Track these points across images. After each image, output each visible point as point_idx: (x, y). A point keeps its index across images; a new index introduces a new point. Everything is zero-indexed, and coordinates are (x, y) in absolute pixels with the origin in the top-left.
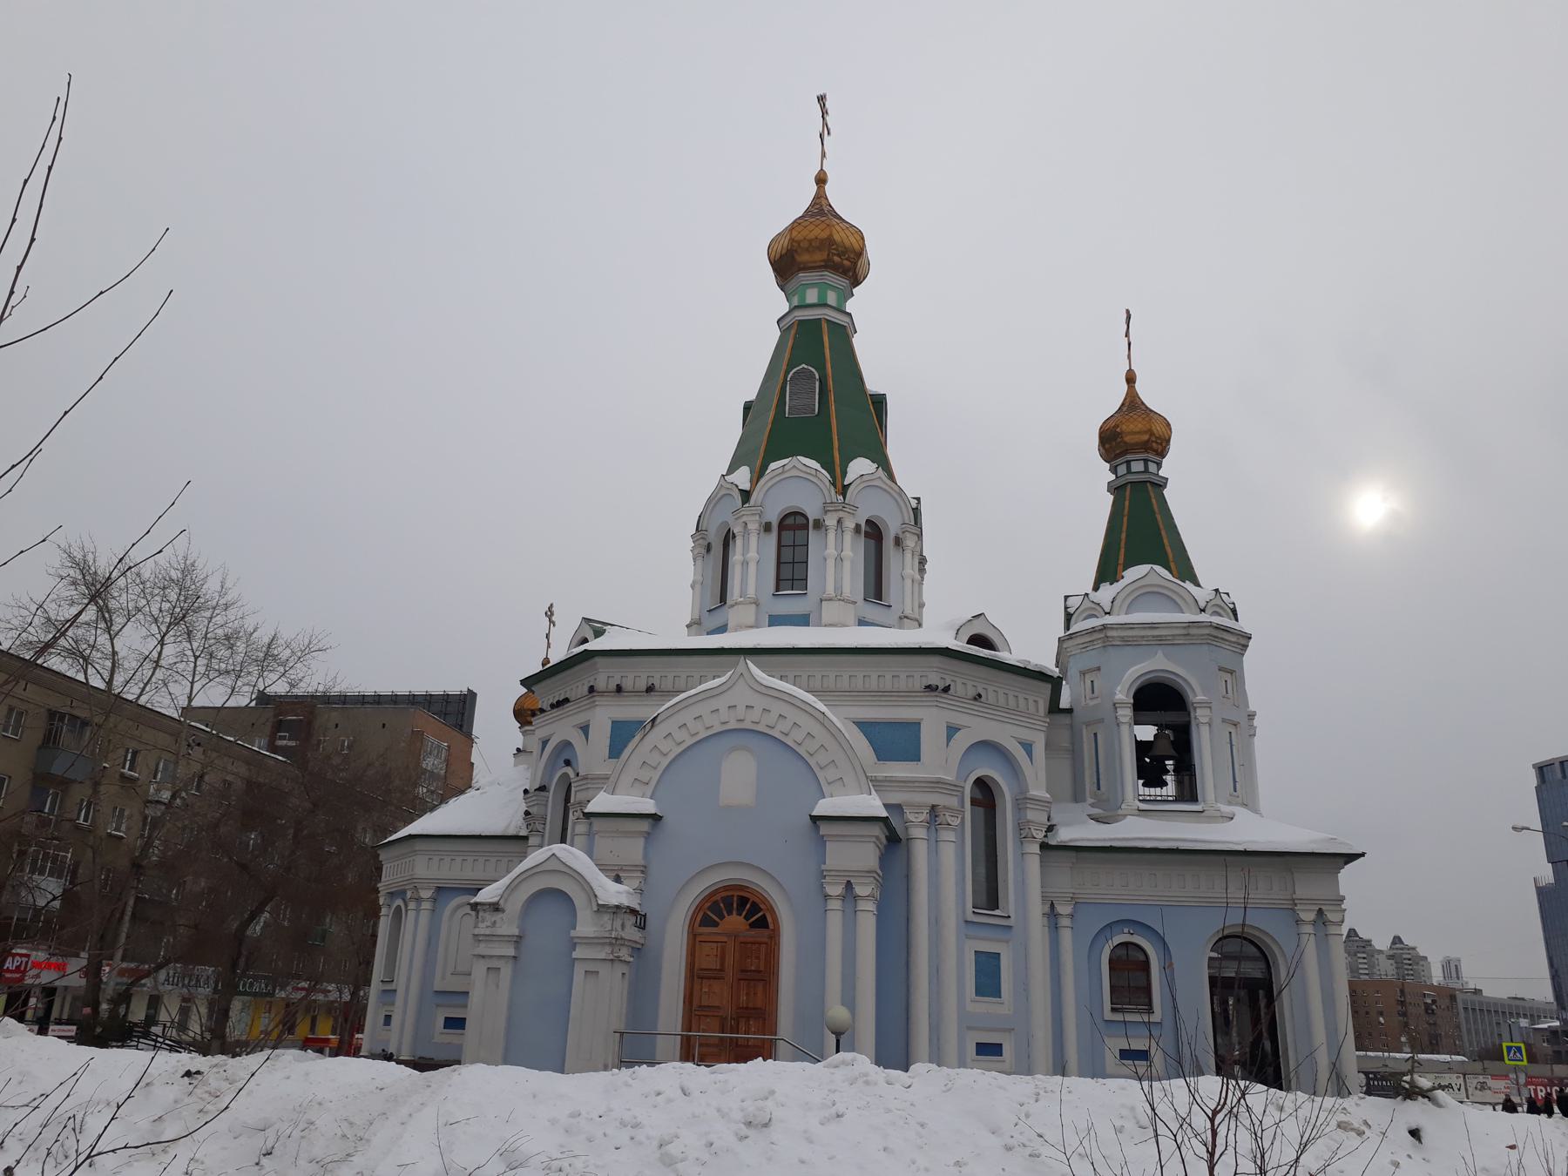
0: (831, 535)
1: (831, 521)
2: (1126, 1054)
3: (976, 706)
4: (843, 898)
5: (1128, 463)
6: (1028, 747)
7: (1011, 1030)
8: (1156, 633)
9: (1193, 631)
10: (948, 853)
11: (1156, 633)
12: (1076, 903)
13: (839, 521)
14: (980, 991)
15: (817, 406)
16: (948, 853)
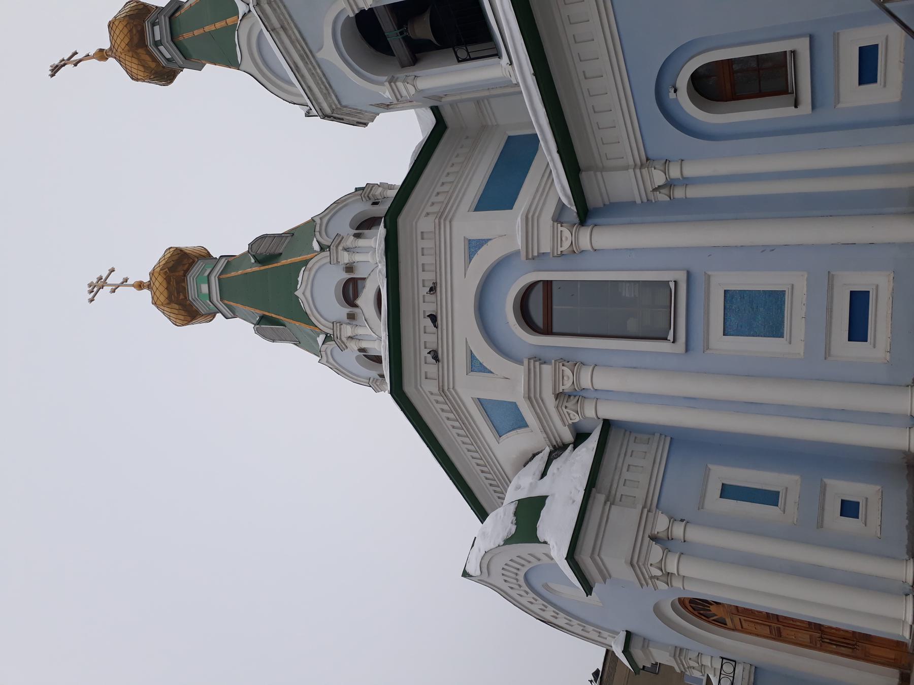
0: (357, 258)
1: (345, 258)
2: (859, 302)
3: (441, 289)
4: (667, 550)
5: (157, 44)
6: (474, 246)
7: (831, 278)
8: (301, 64)
9: (277, 24)
10: (604, 380)
11: (301, 64)
12: (648, 161)
13: (346, 249)
14: (775, 329)
15: (258, 285)
16: (604, 380)
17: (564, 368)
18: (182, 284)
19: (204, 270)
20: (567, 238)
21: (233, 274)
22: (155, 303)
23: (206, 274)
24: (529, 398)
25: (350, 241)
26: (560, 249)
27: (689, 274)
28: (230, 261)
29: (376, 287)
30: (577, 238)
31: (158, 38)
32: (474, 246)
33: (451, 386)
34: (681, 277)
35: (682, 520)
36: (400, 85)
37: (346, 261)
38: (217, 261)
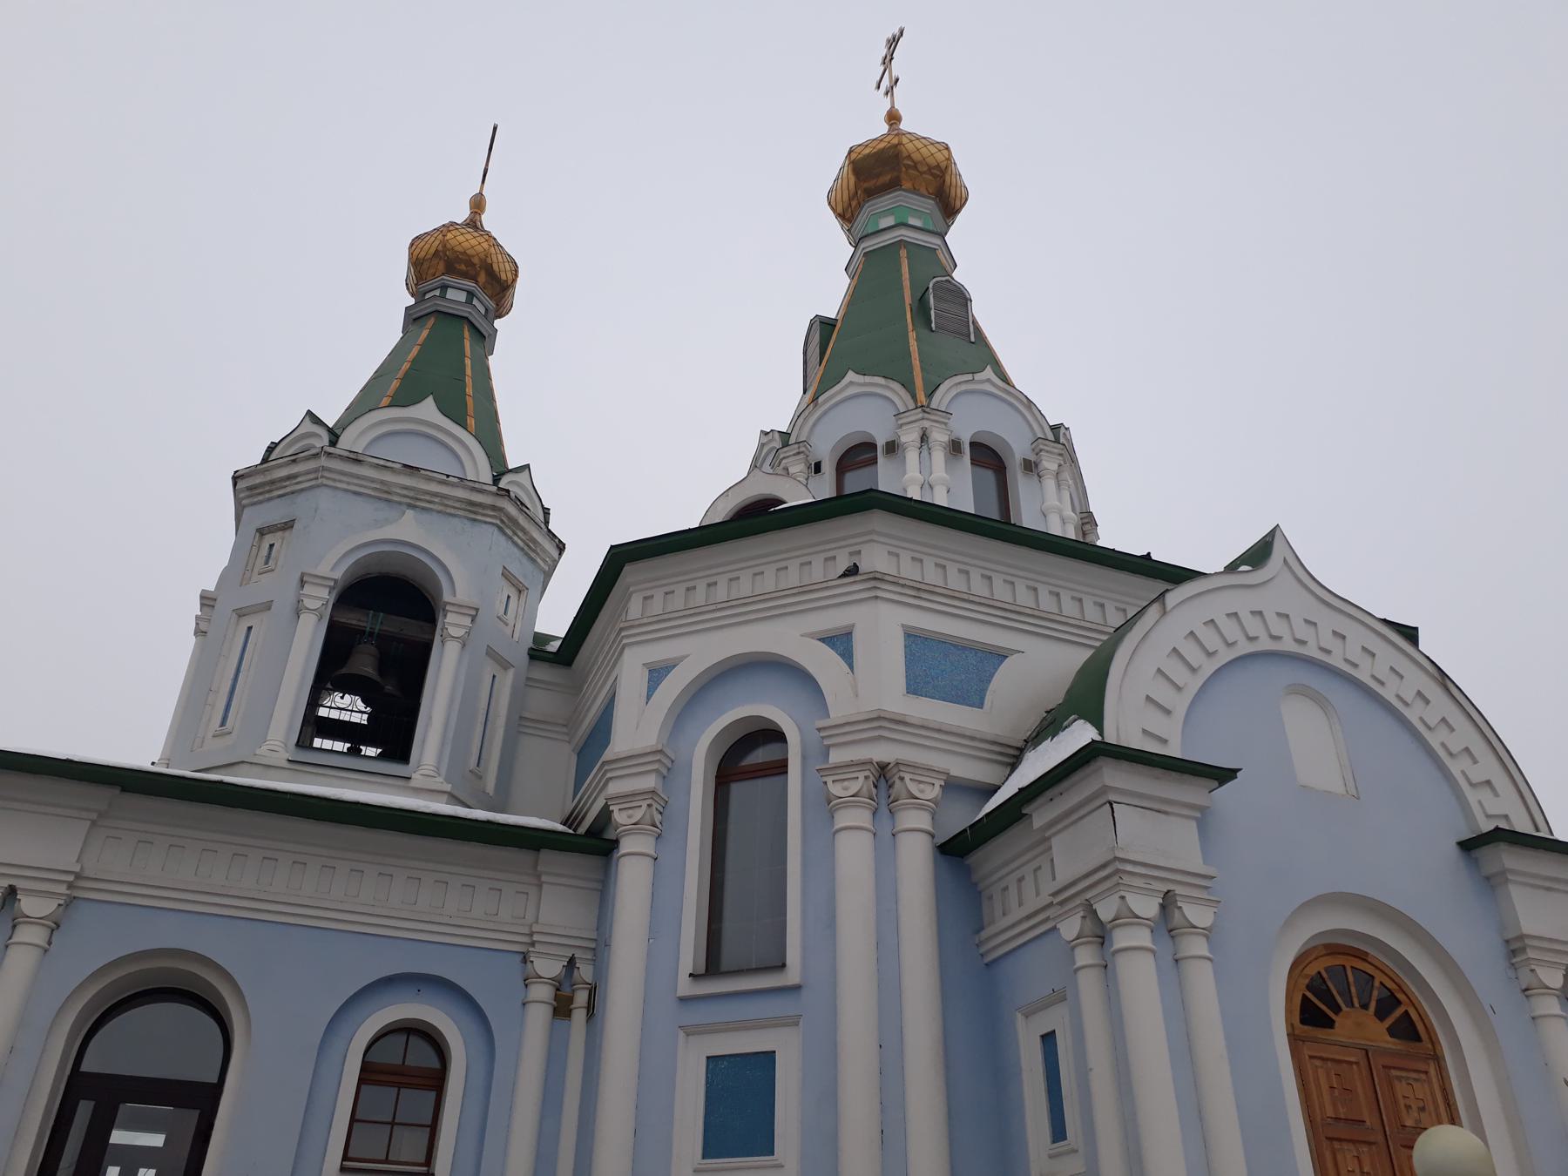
0: (912, 457)
1: (909, 437)
3: (853, 586)
5: (444, 288)
6: (841, 642)
17: (861, 779)
18: (897, 186)
19: (917, 213)
20: (922, 791)
21: (467, 344)
22: (851, 151)
23: (912, 221)
24: (879, 718)
25: (939, 437)
26: (907, 777)
27: (796, 988)
28: (485, 339)
29: (785, 498)
30: (921, 807)
31: (451, 294)
32: (841, 642)
33: (880, 594)
34: (792, 976)
35: (50, 943)
36: (324, 593)
37: (903, 439)
38: (942, 236)
